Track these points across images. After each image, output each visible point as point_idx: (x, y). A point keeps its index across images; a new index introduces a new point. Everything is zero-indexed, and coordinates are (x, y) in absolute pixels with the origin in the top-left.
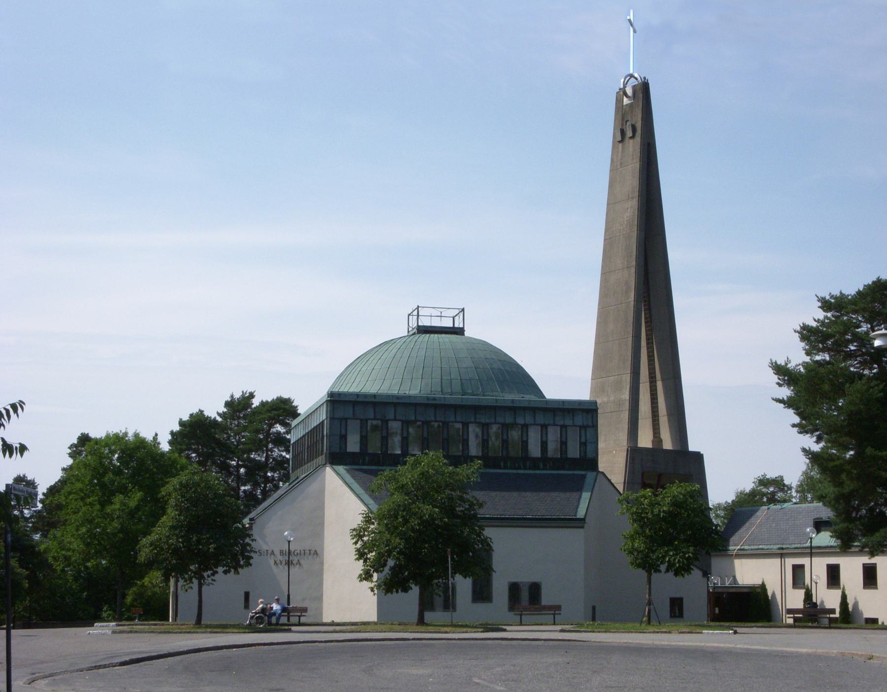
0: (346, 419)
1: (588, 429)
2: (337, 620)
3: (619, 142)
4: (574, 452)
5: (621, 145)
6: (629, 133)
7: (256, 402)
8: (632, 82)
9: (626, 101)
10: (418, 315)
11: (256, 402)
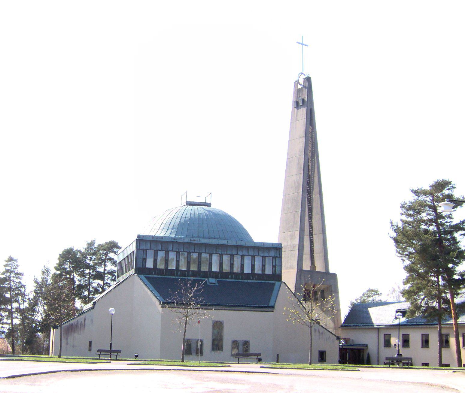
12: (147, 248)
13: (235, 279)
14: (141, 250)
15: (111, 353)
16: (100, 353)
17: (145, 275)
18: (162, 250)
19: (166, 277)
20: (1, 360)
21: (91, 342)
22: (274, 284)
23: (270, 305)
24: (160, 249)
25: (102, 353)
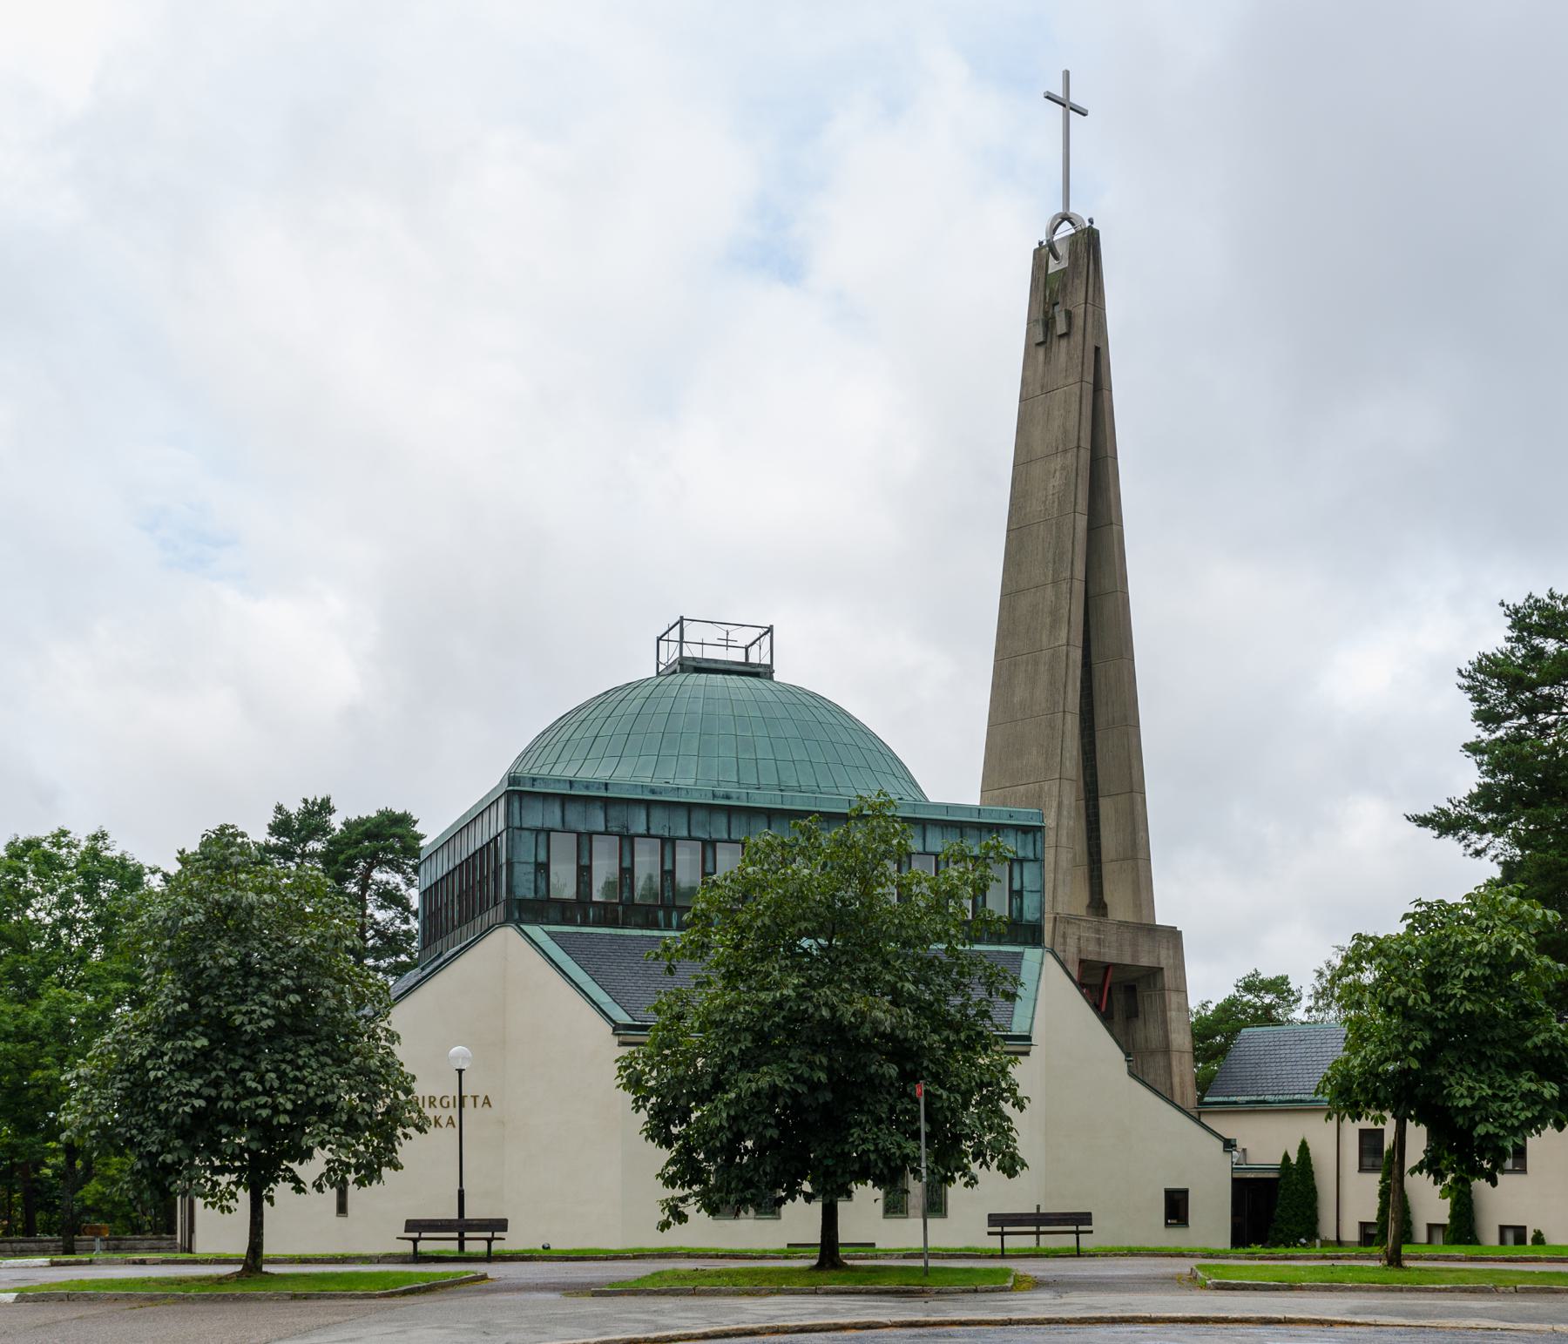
0: (548, 831)
1: (1026, 866)
2: (558, 1245)
3: (1039, 344)
4: (997, 904)
5: (1041, 351)
6: (1061, 327)
7: (336, 822)
8: (1066, 230)
9: (1054, 266)
10: (681, 641)
11: (336, 822)
12: (548, 825)
13: (596, 924)
14: (526, 833)
15: (461, 1234)
16: (416, 1235)
17: (547, 928)
18: (607, 833)
19: (627, 932)
20: (1563, 1261)
21: (1185, 1192)
22: (1021, 955)
23: (1016, 1032)
24: (602, 829)
25: (424, 1235)
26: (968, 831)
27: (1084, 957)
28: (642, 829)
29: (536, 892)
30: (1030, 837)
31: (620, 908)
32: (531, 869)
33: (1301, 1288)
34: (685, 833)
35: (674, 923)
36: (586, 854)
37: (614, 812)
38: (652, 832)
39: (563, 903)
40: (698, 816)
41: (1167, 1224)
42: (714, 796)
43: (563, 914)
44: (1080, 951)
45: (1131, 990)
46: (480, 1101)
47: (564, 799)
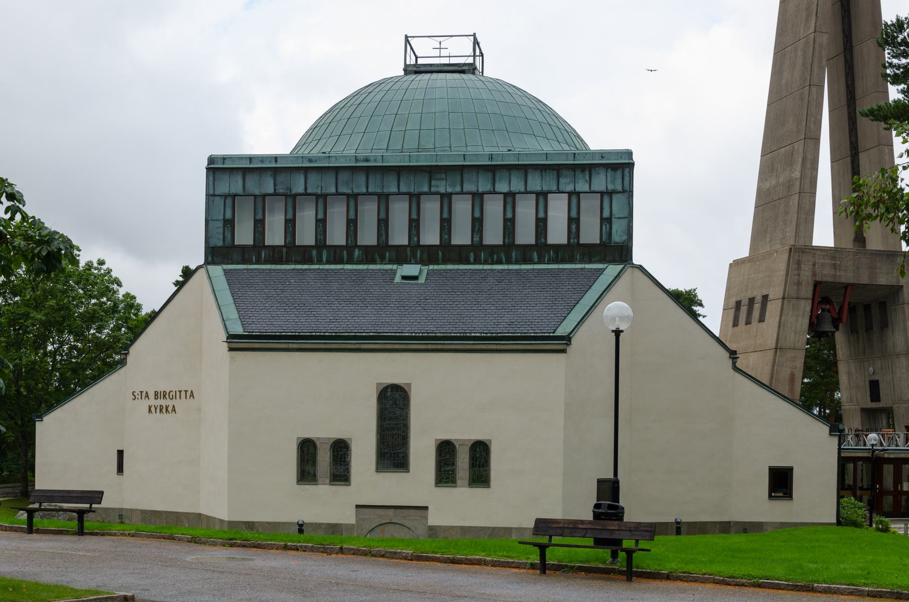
0: (234, 196)
1: (615, 197)
12: (233, 191)
14: (217, 198)
26: (564, 172)
27: (819, 279)
28: (301, 190)
29: (224, 241)
30: (619, 173)
31: (284, 250)
32: (221, 224)
33: (668, 577)
34: (333, 190)
35: (324, 258)
36: (260, 211)
37: (281, 178)
38: (309, 191)
39: (243, 248)
40: (343, 176)
41: (770, 497)
42: (357, 160)
43: (243, 256)
44: (814, 274)
45: (883, 306)
46: (189, 394)
47: (245, 171)
